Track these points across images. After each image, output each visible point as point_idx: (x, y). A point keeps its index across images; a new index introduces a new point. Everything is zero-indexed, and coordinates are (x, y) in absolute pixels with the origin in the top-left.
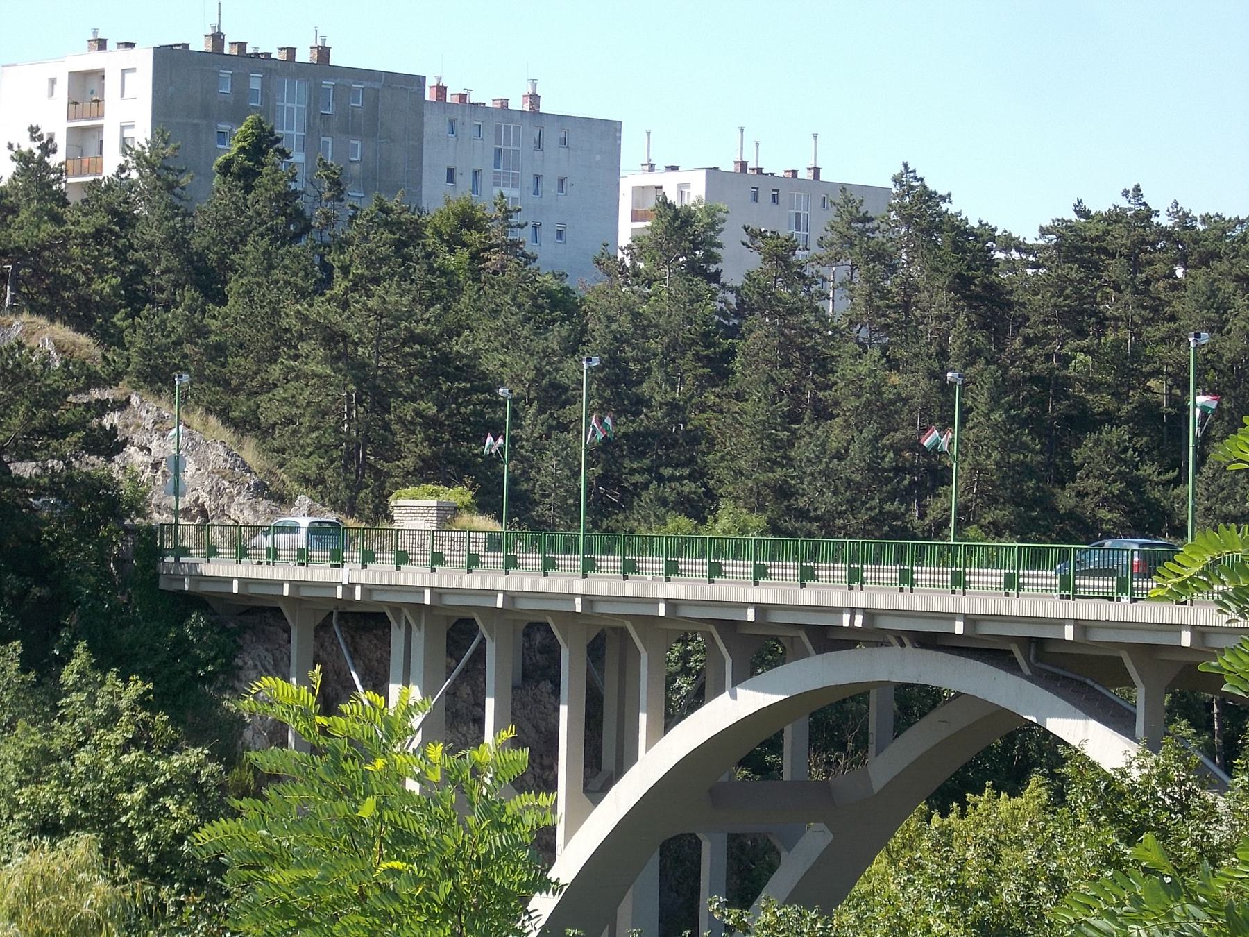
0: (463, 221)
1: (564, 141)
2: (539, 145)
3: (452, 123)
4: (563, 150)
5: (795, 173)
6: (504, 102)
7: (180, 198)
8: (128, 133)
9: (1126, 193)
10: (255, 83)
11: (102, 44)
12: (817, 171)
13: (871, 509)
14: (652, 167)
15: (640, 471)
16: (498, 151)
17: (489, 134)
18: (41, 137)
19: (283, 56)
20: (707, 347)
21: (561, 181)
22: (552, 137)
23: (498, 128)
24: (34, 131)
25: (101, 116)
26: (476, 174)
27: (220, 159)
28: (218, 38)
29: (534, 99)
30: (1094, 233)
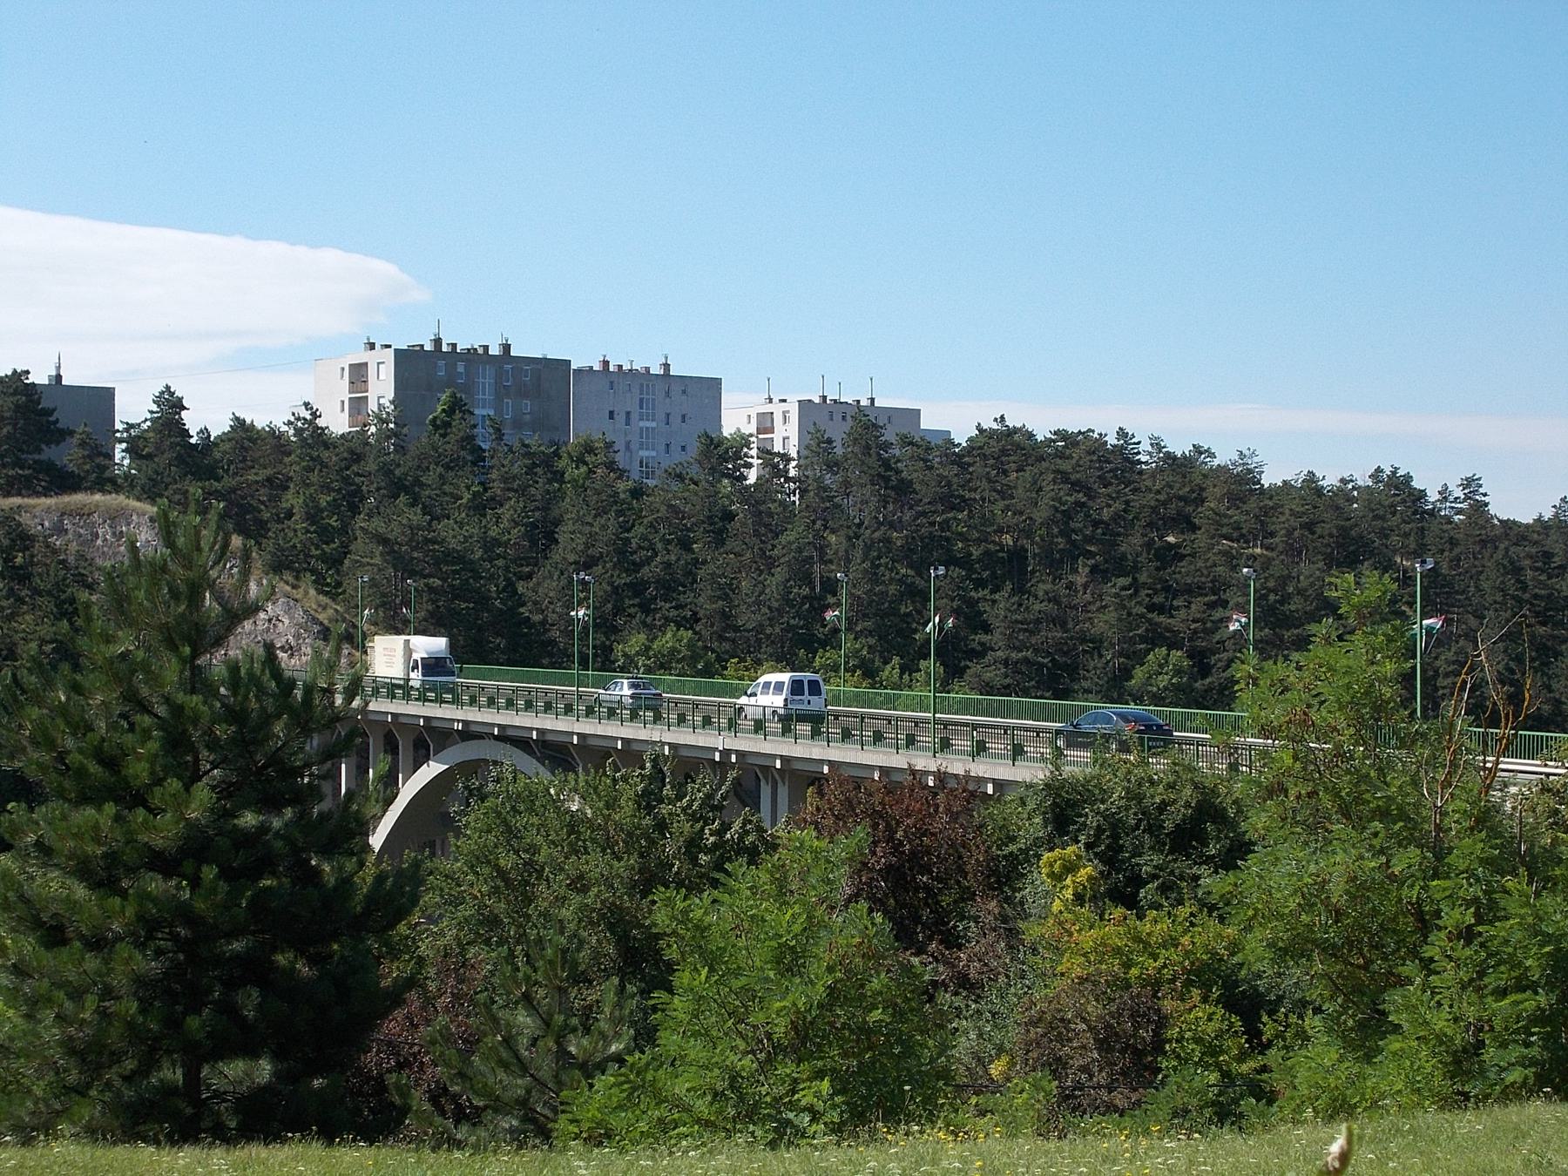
0: (585, 449)
1: (684, 392)
2: (668, 394)
3: (612, 383)
4: (684, 397)
5: (858, 401)
6: (647, 369)
7: (403, 441)
8: (382, 401)
9: (996, 420)
10: (461, 368)
11: (372, 346)
12: (872, 400)
13: (782, 624)
14: (771, 401)
15: (633, 605)
16: (641, 400)
17: (635, 390)
18: (312, 408)
19: (480, 351)
20: (711, 525)
21: (684, 417)
22: (676, 389)
23: (642, 385)
24: (306, 405)
25: (367, 391)
26: (628, 413)
27: (431, 417)
28: (438, 342)
29: (666, 366)
30: (979, 444)
